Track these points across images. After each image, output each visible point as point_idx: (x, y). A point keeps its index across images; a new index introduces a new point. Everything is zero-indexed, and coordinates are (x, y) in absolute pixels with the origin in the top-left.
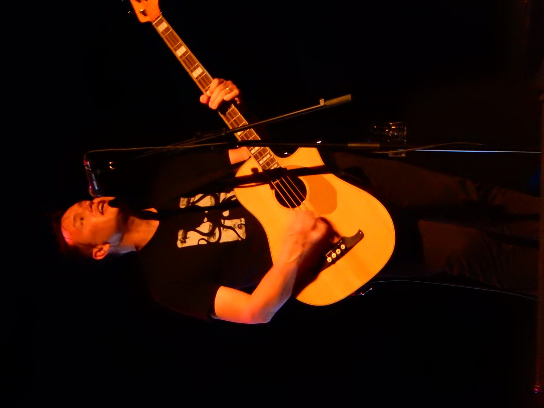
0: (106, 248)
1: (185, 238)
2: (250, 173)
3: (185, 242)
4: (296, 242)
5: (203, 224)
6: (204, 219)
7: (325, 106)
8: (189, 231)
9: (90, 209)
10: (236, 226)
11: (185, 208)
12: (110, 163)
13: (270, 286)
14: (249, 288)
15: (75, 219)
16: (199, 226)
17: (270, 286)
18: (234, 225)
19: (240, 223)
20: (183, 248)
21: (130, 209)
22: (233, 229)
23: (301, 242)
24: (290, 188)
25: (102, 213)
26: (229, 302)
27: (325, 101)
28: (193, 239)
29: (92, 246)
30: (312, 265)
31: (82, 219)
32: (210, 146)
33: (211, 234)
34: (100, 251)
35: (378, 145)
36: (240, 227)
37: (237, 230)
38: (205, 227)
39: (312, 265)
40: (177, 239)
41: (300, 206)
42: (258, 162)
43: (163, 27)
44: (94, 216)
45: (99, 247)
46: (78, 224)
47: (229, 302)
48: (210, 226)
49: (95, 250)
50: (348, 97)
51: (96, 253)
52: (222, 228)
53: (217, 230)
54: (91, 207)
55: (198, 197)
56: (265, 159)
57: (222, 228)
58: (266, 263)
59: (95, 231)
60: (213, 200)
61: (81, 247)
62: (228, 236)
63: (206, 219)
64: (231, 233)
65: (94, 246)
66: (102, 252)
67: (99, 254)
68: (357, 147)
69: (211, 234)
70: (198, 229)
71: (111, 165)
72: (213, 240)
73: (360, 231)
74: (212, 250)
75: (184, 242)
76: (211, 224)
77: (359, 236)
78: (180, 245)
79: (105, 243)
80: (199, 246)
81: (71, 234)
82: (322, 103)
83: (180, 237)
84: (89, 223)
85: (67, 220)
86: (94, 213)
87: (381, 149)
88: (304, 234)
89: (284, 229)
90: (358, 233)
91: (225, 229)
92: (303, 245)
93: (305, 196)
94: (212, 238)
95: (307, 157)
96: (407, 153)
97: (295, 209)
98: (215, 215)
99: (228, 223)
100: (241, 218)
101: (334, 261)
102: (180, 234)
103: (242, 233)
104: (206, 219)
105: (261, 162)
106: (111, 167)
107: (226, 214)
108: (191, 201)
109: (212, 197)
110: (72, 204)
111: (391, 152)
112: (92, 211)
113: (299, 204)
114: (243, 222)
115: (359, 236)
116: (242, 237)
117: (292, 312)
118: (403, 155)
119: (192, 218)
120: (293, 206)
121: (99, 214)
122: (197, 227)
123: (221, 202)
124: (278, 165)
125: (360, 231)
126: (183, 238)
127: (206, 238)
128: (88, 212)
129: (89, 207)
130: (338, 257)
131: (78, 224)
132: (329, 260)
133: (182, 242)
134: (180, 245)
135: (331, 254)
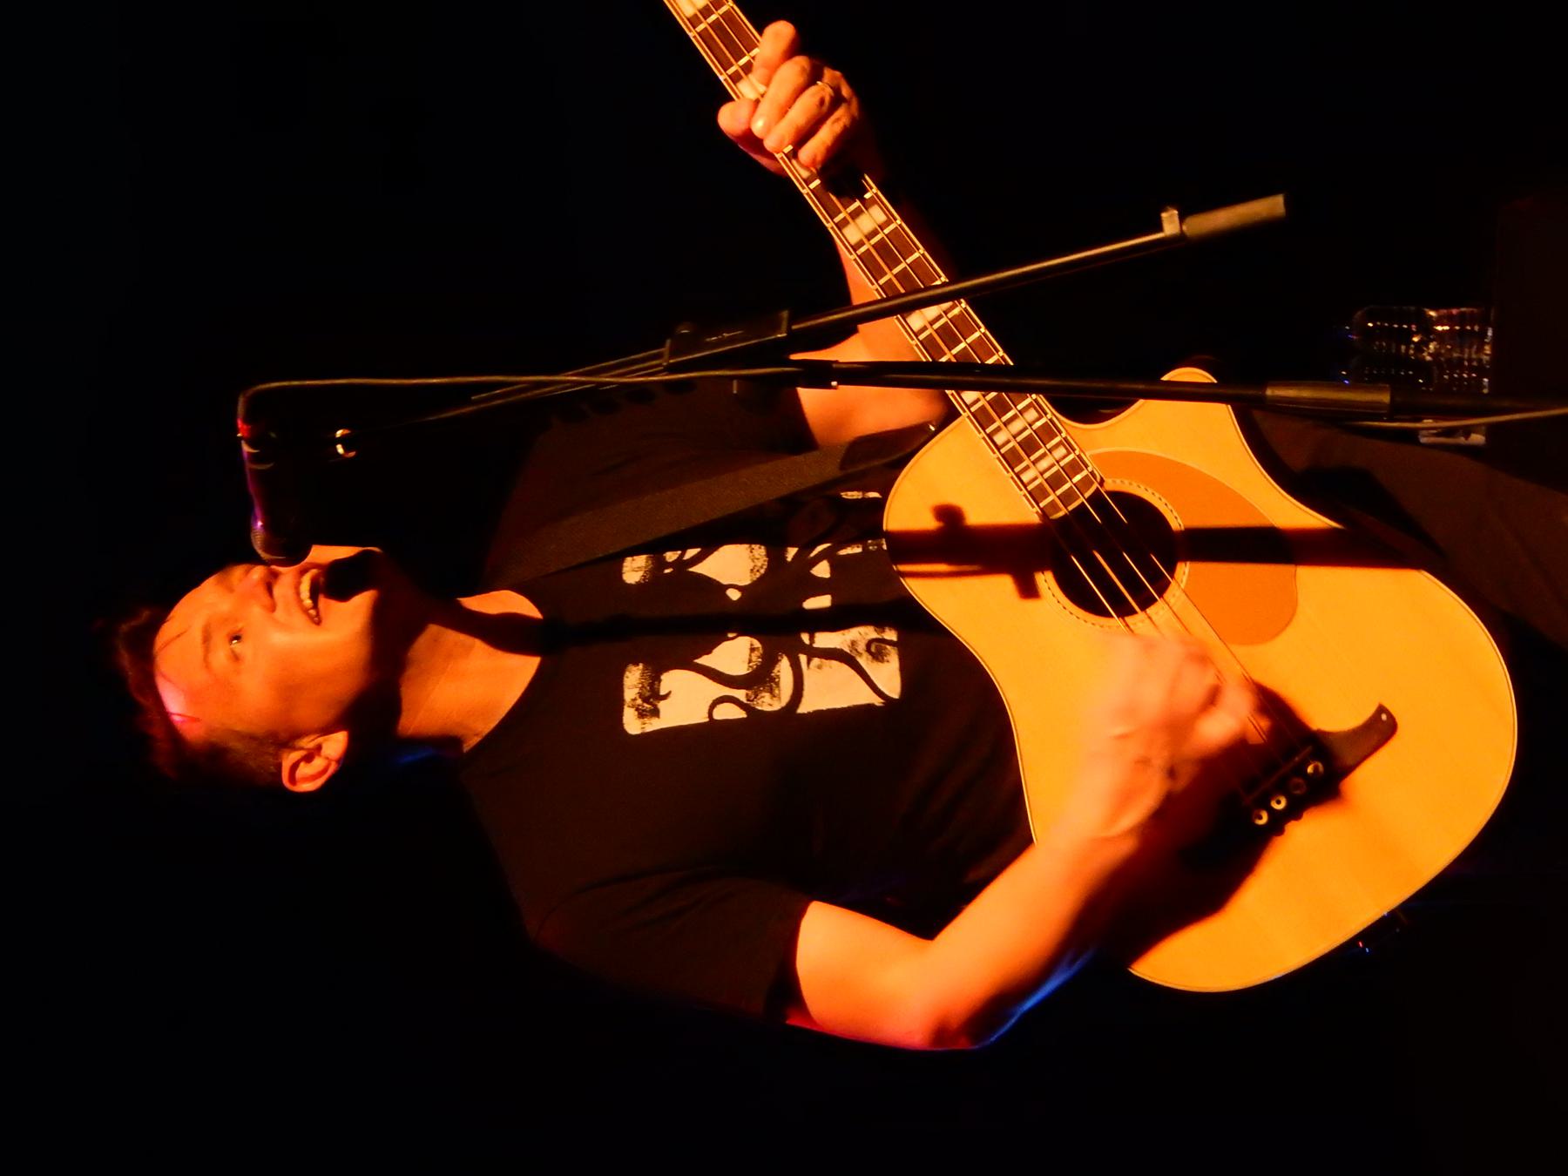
1: (652, 698)
2: (929, 523)
3: (655, 713)
4: (1144, 762)
5: (726, 643)
8: (667, 669)
9: (265, 598)
10: (861, 647)
11: (638, 584)
12: (339, 433)
13: (1005, 927)
14: (923, 910)
15: (207, 639)
16: (709, 653)
18: (853, 643)
20: (645, 737)
21: (413, 597)
23: (1159, 760)
24: (1107, 552)
25: (317, 621)
26: (864, 971)
27: (1182, 219)
28: (687, 699)
29: (284, 739)
31: (238, 638)
32: (673, 354)
33: (760, 678)
34: (308, 758)
35: (1385, 398)
36: (876, 650)
37: (864, 661)
41: (1151, 610)
42: (990, 436)
44: (285, 627)
45: (308, 743)
46: (220, 657)
47: (864, 971)
48: (753, 650)
50: (1272, 206)
51: (295, 767)
52: (803, 658)
54: (269, 588)
55: (691, 553)
57: (803, 658)
58: (1001, 832)
59: (289, 689)
61: (238, 745)
62: (830, 689)
64: (843, 679)
65: (284, 739)
66: (318, 763)
67: (304, 770)
68: (1317, 402)
69: (760, 678)
70: (704, 660)
71: (342, 440)
72: (768, 703)
73: (1381, 709)
74: (778, 753)
76: (757, 644)
77: (1380, 729)
78: (633, 724)
81: (193, 696)
82: (1171, 224)
84: (250, 651)
85: (174, 649)
86: (279, 613)
87: (1394, 412)
89: (1087, 709)
90: (1375, 718)
91: (816, 661)
92: (1172, 773)
95: (1184, 447)
96: (1491, 430)
98: (776, 619)
99: (824, 640)
102: (633, 678)
103: (889, 677)
105: (1000, 438)
106: (340, 449)
110: (195, 582)
111: (1428, 422)
112: (273, 608)
113: (1146, 602)
115: (1380, 729)
118: (1477, 439)
119: (683, 624)
120: (1124, 611)
121: (299, 619)
124: (1070, 448)
125: (1381, 709)
127: (740, 694)
128: (256, 611)
129: (261, 591)
131: (220, 657)
133: (642, 714)
134: (633, 724)
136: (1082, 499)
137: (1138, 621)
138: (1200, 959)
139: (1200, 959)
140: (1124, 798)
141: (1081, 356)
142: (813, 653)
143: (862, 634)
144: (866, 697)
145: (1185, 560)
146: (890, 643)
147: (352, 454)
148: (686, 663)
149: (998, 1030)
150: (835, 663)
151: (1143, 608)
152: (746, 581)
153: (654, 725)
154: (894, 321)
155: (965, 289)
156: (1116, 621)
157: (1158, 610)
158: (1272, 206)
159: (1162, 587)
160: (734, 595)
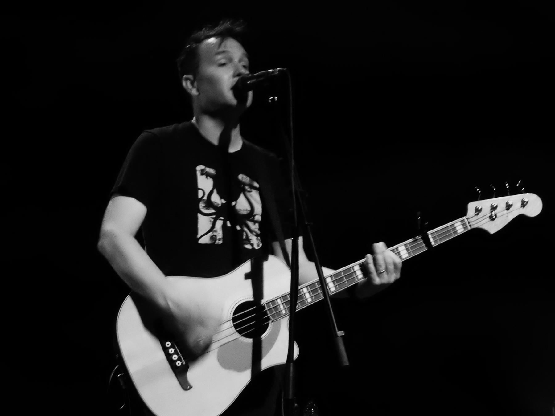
0: (194, 92)
1: (208, 175)
3: (202, 174)
6: (225, 199)
7: (337, 336)
10: (215, 233)
13: (140, 263)
17: (140, 263)
18: (216, 231)
19: (218, 237)
20: (195, 171)
22: (212, 229)
24: (252, 319)
26: (125, 215)
28: (205, 184)
30: (163, 324)
33: (209, 204)
36: (213, 238)
37: (211, 234)
38: (216, 199)
39: (163, 324)
40: (207, 166)
41: (233, 328)
42: (280, 298)
43: (459, 227)
47: (125, 215)
48: (218, 204)
49: (191, 77)
50: (346, 361)
52: (214, 216)
53: (212, 211)
56: (282, 307)
57: (214, 216)
58: (170, 268)
60: (245, 213)
62: (204, 223)
63: (224, 202)
64: (207, 228)
70: (215, 191)
71: (273, 99)
72: (202, 205)
73: (191, 387)
74: (190, 204)
75: (203, 173)
77: (185, 386)
78: (199, 168)
79: (198, 90)
80: (195, 188)
82: (340, 333)
83: (208, 170)
84: (224, 64)
88: (201, 323)
91: (212, 220)
93: (243, 336)
94: (204, 205)
95: (278, 350)
97: (232, 321)
100: (223, 241)
101: (165, 349)
102: (211, 171)
103: (205, 240)
104: (224, 202)
105: (279, 300)
107: (229, 224)
108: (247, 187)
109: (248, 212)
113: (236, 326)
114: (217, 242)
115: (185, 386)
116: (201, 239)
117: (118, 286)
119: (229, 188)
120: (234, 320)
122: (217, 190)
123: (238, 126)
126: (206, 172)
127: (205, 198)
130: (168, 356)
132: (168, 344)
135: (178, 354)
136: (269, 315)
137: (231, 323)
138: (128, 318)
139: (128, 318)
140: (178, 305)
141: (306, 324)
142: (215, 220)
143: (219, 234)
144: (200, 232)
145: (253, 341)
146: (215, 242)
147: (270, 101)
148: (214, 186)
149: (167, 97)
150: (211, 225)
151: (234, 326)
152: (238, 207)
153: (198, 174)
154: (317, 279)
155: (327, 300)
156: (231, 317)
157: (233, 330)
158: (346, 361)
159: (240, 332)
160: (233, 203)
